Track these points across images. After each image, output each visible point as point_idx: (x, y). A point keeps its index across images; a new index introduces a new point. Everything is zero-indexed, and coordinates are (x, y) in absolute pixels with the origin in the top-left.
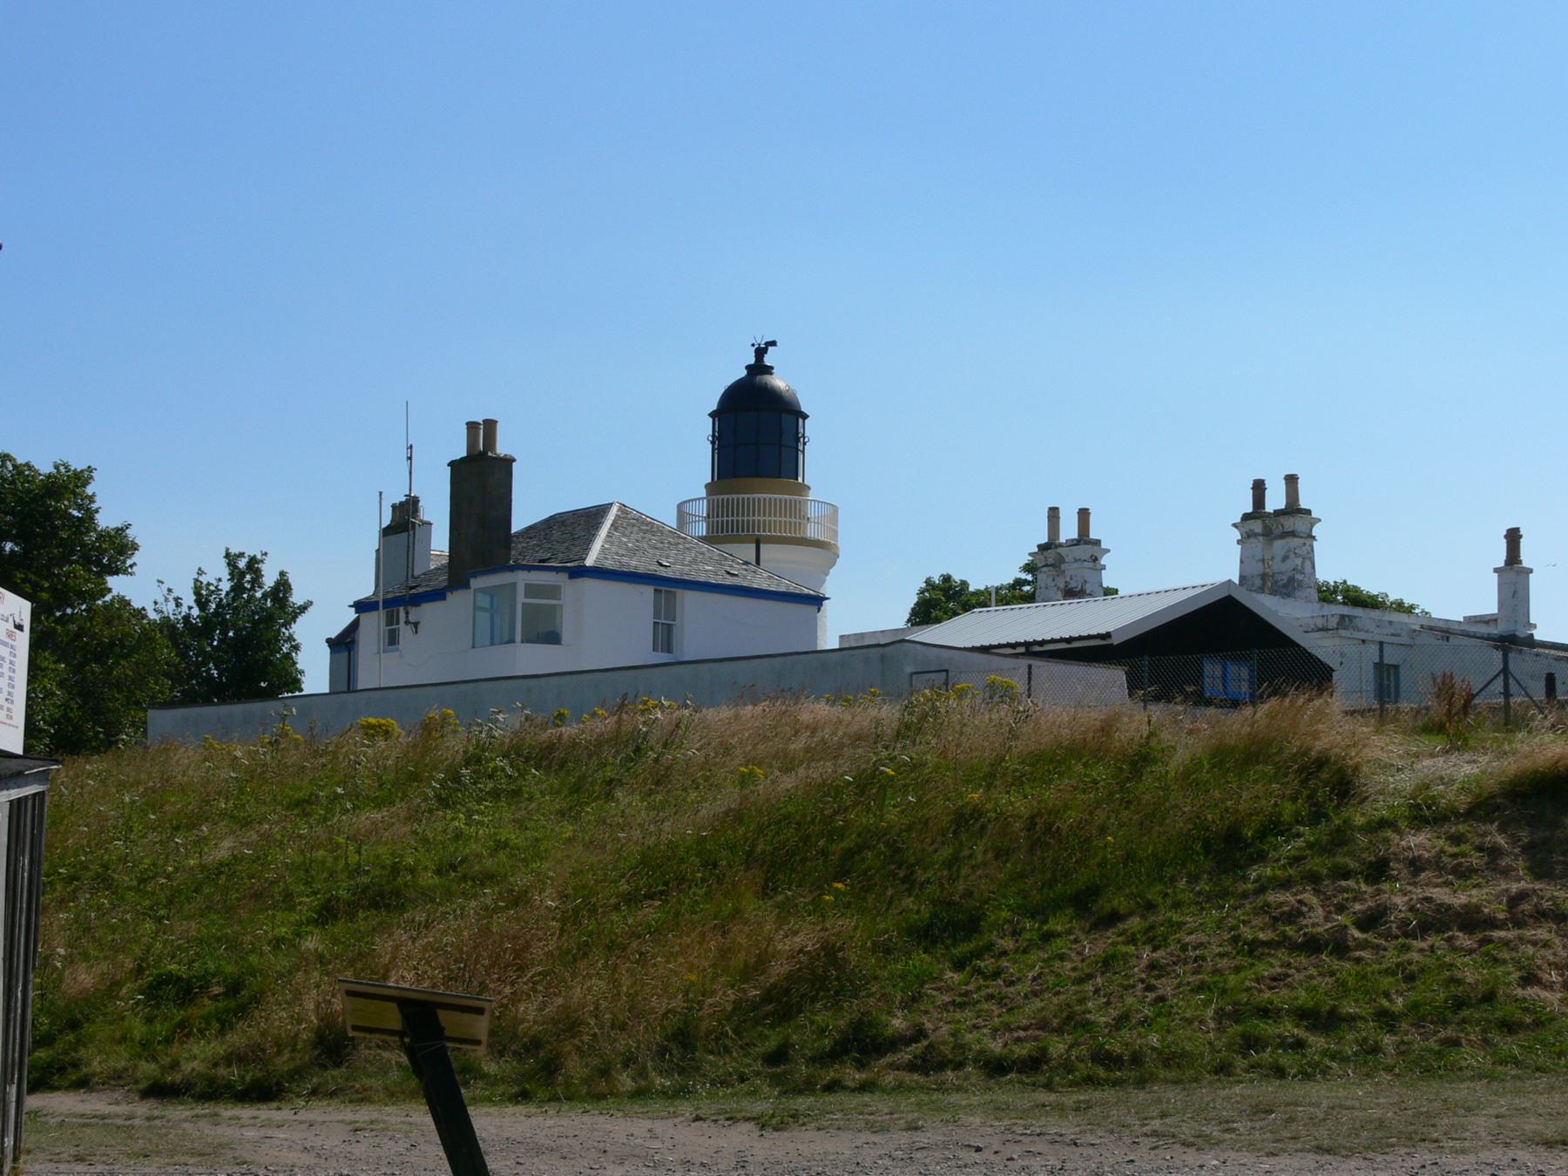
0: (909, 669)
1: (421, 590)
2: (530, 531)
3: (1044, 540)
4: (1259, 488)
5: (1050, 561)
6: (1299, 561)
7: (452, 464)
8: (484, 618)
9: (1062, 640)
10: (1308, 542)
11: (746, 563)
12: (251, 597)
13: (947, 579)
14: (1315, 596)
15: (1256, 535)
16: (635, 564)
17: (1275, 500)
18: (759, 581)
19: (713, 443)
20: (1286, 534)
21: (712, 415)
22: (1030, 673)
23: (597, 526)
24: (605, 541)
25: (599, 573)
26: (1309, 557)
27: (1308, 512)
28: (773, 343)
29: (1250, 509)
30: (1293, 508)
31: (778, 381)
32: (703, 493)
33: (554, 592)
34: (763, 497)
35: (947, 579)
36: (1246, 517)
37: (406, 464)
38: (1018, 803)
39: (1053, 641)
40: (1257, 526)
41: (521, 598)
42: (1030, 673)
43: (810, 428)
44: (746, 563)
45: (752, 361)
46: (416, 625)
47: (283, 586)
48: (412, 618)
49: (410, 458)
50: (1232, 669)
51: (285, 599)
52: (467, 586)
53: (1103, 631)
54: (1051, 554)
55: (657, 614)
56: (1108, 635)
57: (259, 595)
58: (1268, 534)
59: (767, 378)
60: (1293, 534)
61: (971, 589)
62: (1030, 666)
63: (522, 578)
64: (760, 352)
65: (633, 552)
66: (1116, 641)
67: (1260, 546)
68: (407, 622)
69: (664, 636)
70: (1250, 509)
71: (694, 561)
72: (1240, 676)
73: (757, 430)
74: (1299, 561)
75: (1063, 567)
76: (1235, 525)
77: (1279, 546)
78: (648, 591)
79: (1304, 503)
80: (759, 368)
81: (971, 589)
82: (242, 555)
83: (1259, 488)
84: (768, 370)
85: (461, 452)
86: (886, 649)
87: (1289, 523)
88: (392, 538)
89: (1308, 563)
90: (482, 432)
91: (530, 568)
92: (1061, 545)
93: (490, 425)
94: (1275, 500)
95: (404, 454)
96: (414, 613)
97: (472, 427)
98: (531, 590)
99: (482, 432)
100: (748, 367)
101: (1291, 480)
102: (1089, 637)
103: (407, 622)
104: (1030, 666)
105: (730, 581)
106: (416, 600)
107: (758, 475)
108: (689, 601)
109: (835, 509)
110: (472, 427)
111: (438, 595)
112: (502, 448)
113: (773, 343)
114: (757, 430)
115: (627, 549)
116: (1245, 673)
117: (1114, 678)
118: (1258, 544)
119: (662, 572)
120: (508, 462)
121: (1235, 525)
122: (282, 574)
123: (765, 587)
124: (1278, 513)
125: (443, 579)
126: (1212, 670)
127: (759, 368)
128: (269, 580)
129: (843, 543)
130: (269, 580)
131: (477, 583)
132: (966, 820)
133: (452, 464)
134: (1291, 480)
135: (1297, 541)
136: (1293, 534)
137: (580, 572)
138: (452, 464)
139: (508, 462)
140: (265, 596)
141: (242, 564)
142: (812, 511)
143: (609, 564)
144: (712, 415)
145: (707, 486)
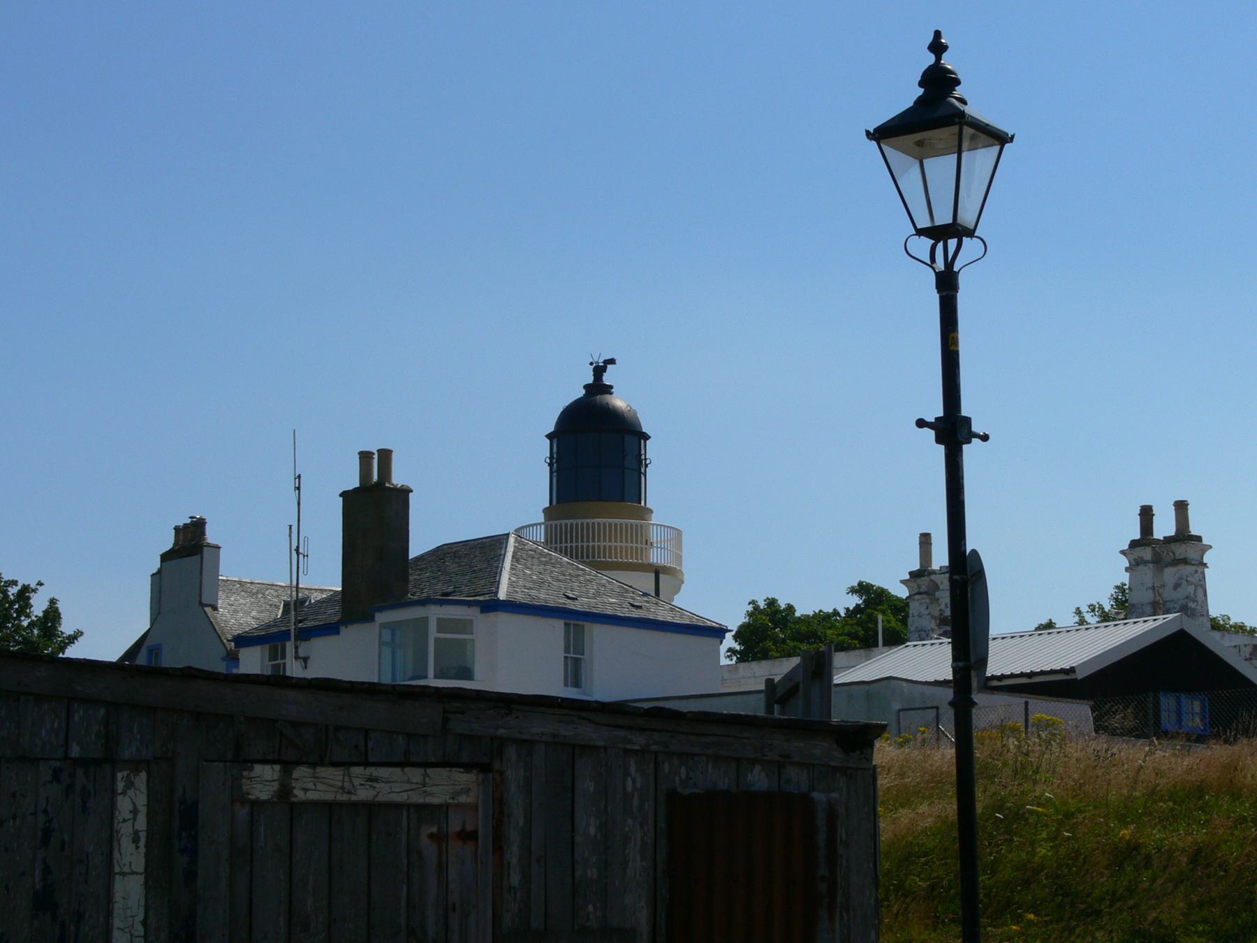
0: (896, 706)
1: (309, 624)
2: (418, 559)
3: (916, 566)
4: (1146, 514)
5: (923, 589)
6: (1191, 589)
7: (344, 494)
8: (387, 651)
9: (1022, 675)
10: (1200, 570)
11: (645, 594)
12: (18, 628)
13: (772, 603)
14: (1208, 625)
15: (1145, 562)
16: (544, 597)
17: (1164, 527)
18: (662, 615)
19: (551, 465)
20: (1177, 562)
21: (550, 436)
22: (1026, 709)
23: (500, 558)
24: (511, 574)
25: (511, 607)
26: (1201, 585)
27: (1199, 539)
28: (612, 361)
29: (1137, 536)
30: (1183, 535)
31: (618, 401)
32: (541, 518)
33: (464, 626)
34: (606, 521)
35: (772, 603)
36: (1134, 544)
37: (294, 494)
38: (1183, 838)
39: (1012, 676)
40: (1147, 553)
41: (433, 633)
42: (1026, 709)
43: (652, 450)
44: (645, 594)
45: (590, 380)
46: (305, 659)
47: (52, 614)
48: (302, 653)
49: (298, 488)
50: (1185, 700)
51: (54, 628)
52: (368, 618)
53: (1067, 666)
54: (924, 582)
55: (567, 650)
56: (1072, 670)
57: (25, 623)
58: (1159, 562)
59: (607, 398)
60: (1185, 561)
61: (797, 614)
62: (1026, 703)
63: (434, 613)
64: (599, 371)
65: (541, 584)
66: (1080, 675)
67: (1150, 574)
68: (297, 658)
69: (575, 671)
70: (1137, 536)
71: (597, 594)
72: (1194, 710)
73: (597, 451)
74: (1191, 589)
75: (938, 594)
76: (1123, 552)
77: (1170, 574)
78: (559, 625)
79: (1194, 530)
80: (598, 388)
81: (797, 614)
82: (15, 583)
83: (1146, 514)
84: (608, 389)
85: (353, 482)
86: (872, 686)
87: (1180, 550)
88: (173, 563)
89: (1200, 592)
90: (377, 464)
91: (441, 603)
92: (934, 572)
93: (385, 455)
94: (1164, 527)
95: (291, 484)
96: (304, 649)
97: (365, 457)
98: (443, 625)
99: (377, 464)
100: (586, 387)
101: (1181, 507)
102: (1052, 672)
103: (297, 658)
104: (1026, 703)
105: (636, 614)
106: (305, 634)
107: (600, 500)
108: (598, 635)
109: (679, 532)
110: (365, 457)
111: (330, 629)
112: (398, 478)
113: (612, 361)
114: (597, 451)
115: (533, 581)
116: (1197, 706)
117: (1077, 714)
118: (1147, 573)
119: (571, 605)
120: (405, 493)
121: (1123, 552)
122: (53, 602)
123: (669, 619)
124: (1168, 540)
125: (333, 614)
126: (1167, 702)
127: (598, 388)
128: (38, 606)
129: (688, 569)
130: (38, 606)
131: (381, 618)
132: (1127, 854)
133: (344, 494)
134: (1181, 507)
135: (1189, 569)
136: (1185, 561)
137: (492, 606)
138: (344, 495)
139: (405, 493)
140: (32, 625)
141: (13, 591)
142: (655, 535)
143: (520, 597)
144: (550, 436)
145: (545, 510)
